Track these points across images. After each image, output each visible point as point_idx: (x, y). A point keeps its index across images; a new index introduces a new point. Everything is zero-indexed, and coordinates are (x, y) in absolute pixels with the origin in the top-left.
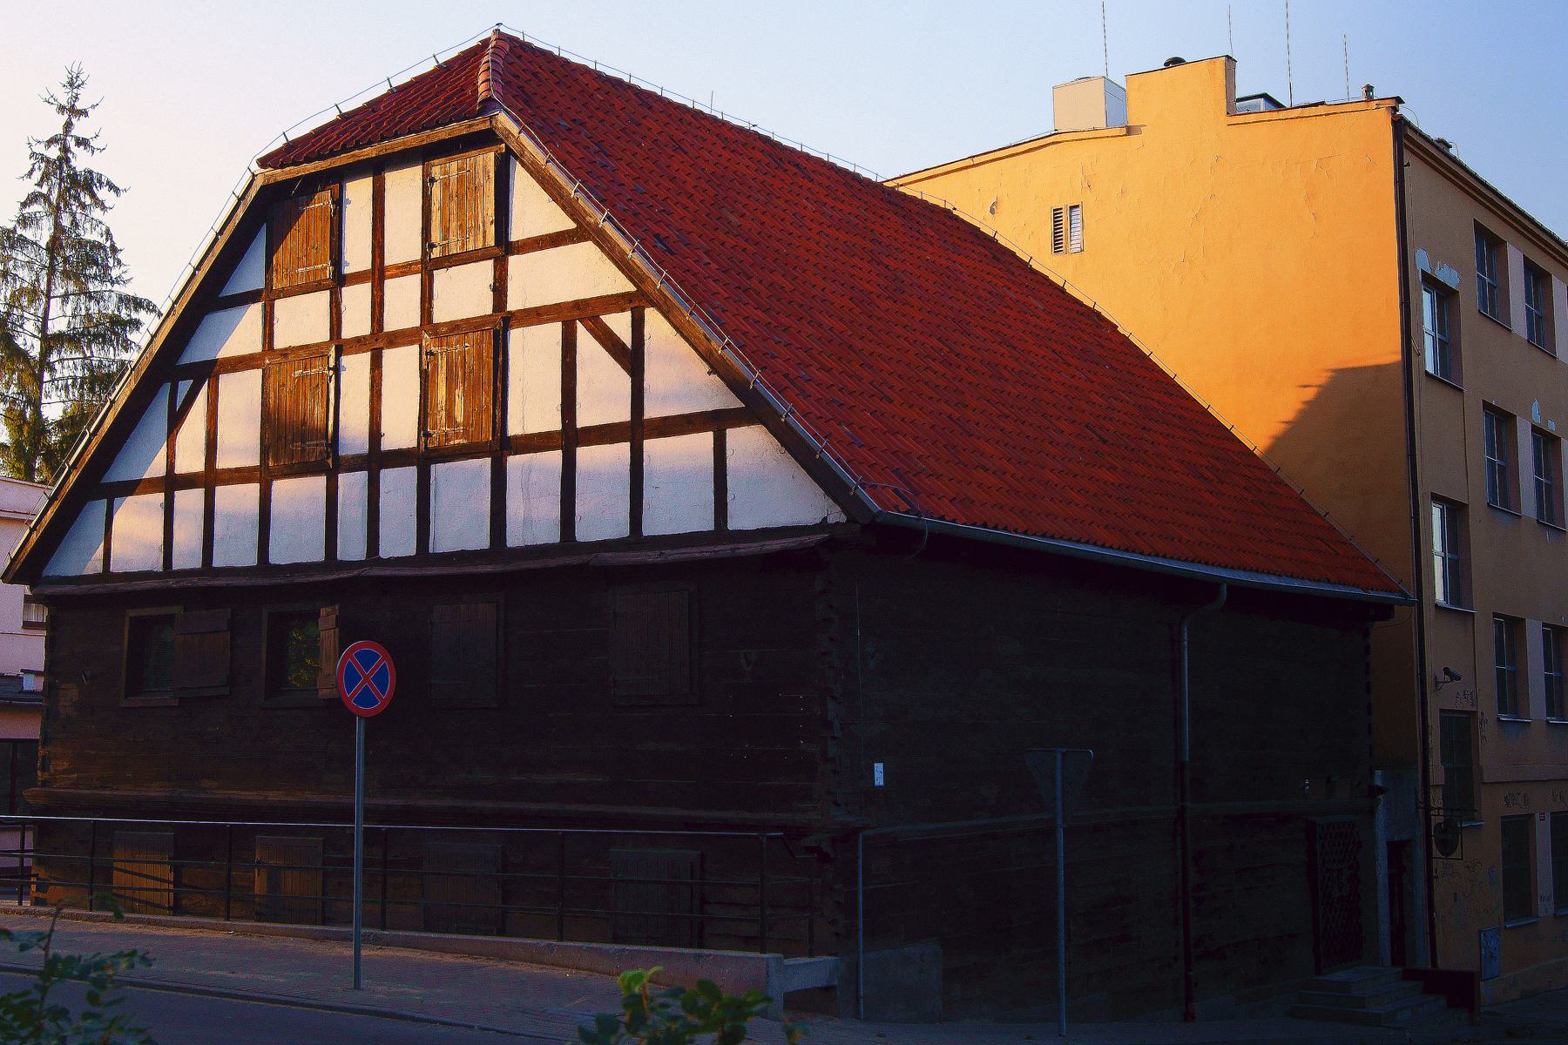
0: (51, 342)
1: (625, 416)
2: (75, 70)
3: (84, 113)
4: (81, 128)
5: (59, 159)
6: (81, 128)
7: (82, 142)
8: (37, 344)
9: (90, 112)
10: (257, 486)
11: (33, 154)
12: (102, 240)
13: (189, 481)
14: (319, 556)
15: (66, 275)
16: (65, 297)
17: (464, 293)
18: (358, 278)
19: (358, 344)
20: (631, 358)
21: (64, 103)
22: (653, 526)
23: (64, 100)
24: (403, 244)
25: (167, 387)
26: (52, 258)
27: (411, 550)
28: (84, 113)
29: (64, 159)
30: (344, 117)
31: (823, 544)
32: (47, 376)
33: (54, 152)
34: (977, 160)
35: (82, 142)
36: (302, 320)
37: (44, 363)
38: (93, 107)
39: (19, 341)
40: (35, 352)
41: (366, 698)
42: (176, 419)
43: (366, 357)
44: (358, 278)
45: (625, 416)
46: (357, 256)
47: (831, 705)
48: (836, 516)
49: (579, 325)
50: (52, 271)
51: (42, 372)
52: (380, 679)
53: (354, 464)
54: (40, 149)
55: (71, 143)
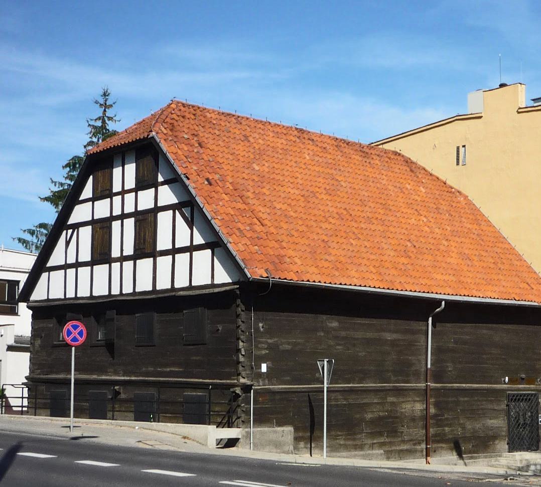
2: (106, 89)
3: (111, 106)
4: (109, 113)
5: (102, 126)
6: (109, 113)
7: (110, 119)
9: (113, 105)
11: (89, 125)
14: (107, 293)
17: (146, 200)
18: (117, 194)
21: (102, 103)
23: (102, 101)
24: (130, 183)
25: (65, 232)
27: (131, 291)
28: (111, 106)
29: (104, 127)
33: (99, 124)
34: (428, 127)
35: (110, 119)
36: (102, 209)
38: (114, 103)
41: (75, 339)
42: (68, 243)
44: (117, 194)
45: (170, 247)
46: (117, 188)
49: (177, 210)
52: (81, 334)
54: (92, 123)
55: (106, 119)
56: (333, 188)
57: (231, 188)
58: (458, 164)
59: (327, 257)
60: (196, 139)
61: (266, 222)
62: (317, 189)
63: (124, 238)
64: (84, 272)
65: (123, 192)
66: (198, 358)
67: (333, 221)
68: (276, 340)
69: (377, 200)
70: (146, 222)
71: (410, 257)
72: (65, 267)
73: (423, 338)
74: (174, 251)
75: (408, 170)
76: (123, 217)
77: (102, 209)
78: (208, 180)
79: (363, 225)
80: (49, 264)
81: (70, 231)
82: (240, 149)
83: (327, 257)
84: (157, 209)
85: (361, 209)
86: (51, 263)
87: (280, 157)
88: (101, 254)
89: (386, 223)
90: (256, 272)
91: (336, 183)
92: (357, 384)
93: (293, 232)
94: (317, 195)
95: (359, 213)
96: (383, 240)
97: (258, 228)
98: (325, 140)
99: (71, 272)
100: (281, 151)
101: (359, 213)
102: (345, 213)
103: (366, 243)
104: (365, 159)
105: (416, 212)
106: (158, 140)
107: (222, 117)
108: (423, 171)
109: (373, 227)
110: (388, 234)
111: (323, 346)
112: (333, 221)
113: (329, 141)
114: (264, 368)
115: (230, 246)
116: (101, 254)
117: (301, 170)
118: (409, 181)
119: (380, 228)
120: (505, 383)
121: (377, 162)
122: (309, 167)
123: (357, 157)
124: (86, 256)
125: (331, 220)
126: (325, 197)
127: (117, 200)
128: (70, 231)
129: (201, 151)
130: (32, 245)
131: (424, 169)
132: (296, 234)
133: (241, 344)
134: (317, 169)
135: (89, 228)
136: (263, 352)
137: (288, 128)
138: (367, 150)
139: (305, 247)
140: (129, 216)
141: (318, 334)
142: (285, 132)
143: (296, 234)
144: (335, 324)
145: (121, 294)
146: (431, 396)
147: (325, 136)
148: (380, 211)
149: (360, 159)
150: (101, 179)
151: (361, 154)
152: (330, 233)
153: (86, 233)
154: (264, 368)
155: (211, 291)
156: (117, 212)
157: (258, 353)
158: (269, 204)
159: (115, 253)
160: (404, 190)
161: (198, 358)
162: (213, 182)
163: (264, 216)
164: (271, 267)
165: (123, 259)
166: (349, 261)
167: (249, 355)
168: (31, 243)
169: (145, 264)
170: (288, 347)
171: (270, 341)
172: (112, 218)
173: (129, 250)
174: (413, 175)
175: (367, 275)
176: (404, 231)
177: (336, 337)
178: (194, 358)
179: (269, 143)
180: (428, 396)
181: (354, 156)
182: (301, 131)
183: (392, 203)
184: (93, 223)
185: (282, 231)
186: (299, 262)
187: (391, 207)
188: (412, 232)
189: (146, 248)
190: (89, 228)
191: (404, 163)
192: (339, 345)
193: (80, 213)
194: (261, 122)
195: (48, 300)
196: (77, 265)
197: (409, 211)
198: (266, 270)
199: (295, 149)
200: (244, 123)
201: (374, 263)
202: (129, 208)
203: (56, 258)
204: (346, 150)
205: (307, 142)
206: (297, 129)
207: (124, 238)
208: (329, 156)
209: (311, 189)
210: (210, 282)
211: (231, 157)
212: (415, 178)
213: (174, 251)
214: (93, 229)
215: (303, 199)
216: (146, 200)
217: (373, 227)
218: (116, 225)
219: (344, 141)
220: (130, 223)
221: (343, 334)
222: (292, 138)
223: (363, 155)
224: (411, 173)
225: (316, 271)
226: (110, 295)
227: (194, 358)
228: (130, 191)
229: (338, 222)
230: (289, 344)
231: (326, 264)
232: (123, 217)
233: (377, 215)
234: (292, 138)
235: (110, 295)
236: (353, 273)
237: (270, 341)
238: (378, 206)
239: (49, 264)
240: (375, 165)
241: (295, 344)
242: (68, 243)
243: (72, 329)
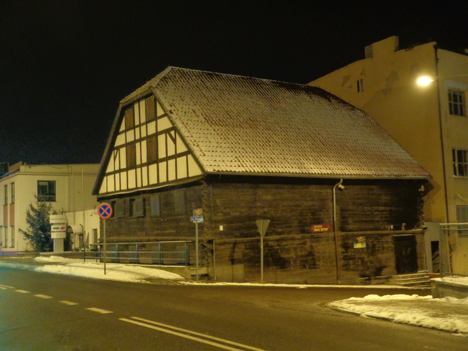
17: (152, 128)
22: (190, 175)
36: (130, 136)
42: (115, 158)
52: (108, 211)
58: (358, 91)
64: (124, 174)
65: (140, 126)
72: (114, 172)
74: (167, 158)
76: (141, 140)
77: (130, 136)
81: (116, 151)
88: (132, 165)
90: (210, 170)
92: (106, 229)
99: (117, 175)
114: (221, 228)
116: (132, 165)
120: (391, 230)
124: (124, 166)
127: (137, 130)
145: (142, 187)
146: (338, 241)
153: (123, 151)
154: (221, 228)
156: (138, 137)
159: (138, 162)
165: (142, 165)
169: (153, 168)
173: (145, 160)
180: (336, 240)
189: (153, 159)
195: (188, 178)
196: (120, 171)
213: (167, 158)
214: (126, 149)
216: (152, 128)
226: (137, 188)
232: (141, 140)
235: (137, 188)
242: (115, 158)
243: (107, 209)
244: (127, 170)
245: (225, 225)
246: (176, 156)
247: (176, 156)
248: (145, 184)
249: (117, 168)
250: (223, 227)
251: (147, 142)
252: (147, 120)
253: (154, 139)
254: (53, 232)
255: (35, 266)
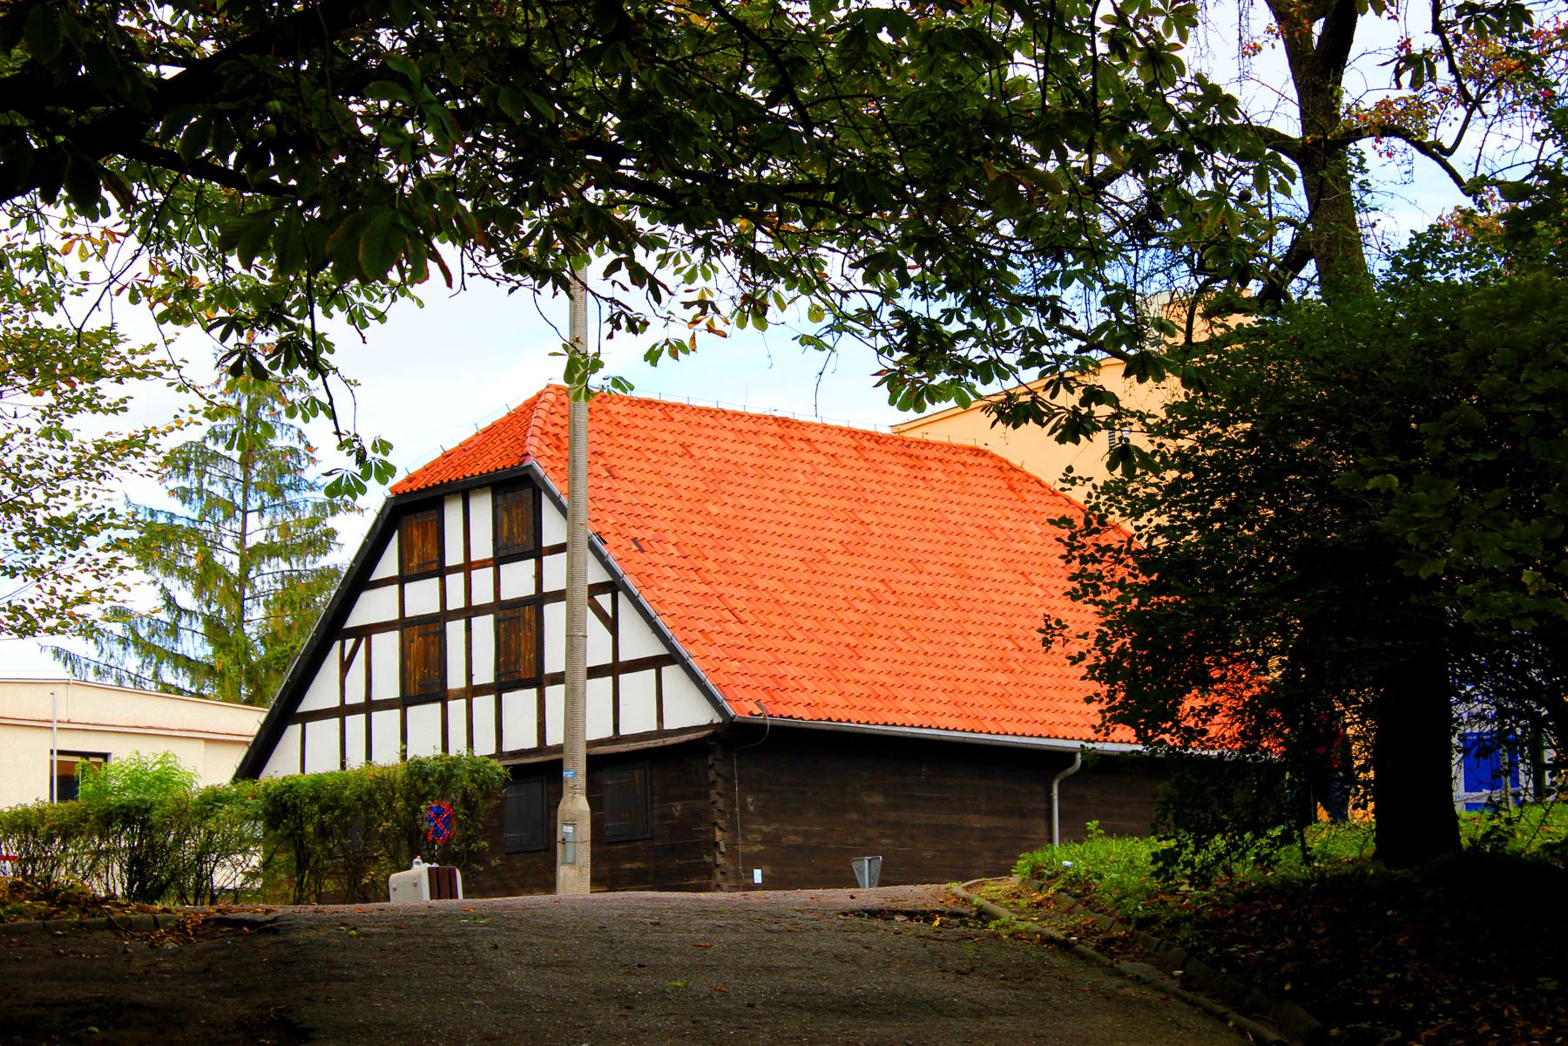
0: (252, 556)
1: (374, 714)
8: (236, 560)
10: (547, 671)
12: (295, 444)
13: (354, 709)
15: (260, 488)
16: (261, 511)
17: (518, 580)
18: (455, 569)
19: (456, 615)
20: (612, 624)
22: (670, 724)
24: (483, 547)
25: (338, 644)
26: (247, 474)
30: (446, 455)
31: (709, 736)
32: (248, 593)
36: (423, 598)
37: (244, 579)
39: (218, 559)
40: (235, 569)
42: (345, 665)
43: (462, 622)
44: (455, 569)
46: (454, 556)
47: (718, 833)
48: (718, 719)
50: (246, 485)
51: (242, 588)
53: (458, 695)
56: (855, 539)
57: (677, 554)
59: (857, 676)
60: (601, 461)
61: (744, 616)
62: (827, 545)
63: (473, 651)
65: (468, 567)
66: (637, 865)
67: (862, 606)
68: (776, 826)
69: (944, 558)
70: (519, 623)
71: (1012, 671)
72: (343, 711)
73: (1043, 824)
75: (1005, 486)
76: (470, 612)
77: (423, 598)
78: (634, 540)
79: (918, 612)
80: (303, 708)
81: (350, 643)
82: (680, 472)
83: (857, 676)
84: (540, 599)
85: (913, 578)
86: (309, 704)
87: (753, 482)
88: (424, 683)
89: (963, 604)
90: (744, 708)
91: (862, 529)
93: (793, 632)
94: (828, 555)
95: (910, 588)
96: (958, 639)
97: (735, 628)
98: (832, 438)
99: (356, 723)
100: (751, 471)
101: (910, 588)
102: (882, 588)
103: (927, 647)
104: (914, 472)
105: (1020, 578)
106: (542, 473)
107: (638, 410)
108: (1036, 487)
109: (938, 615)
110: (969, 627)
111: (858, 840)
112: (862, 606)
113: (840, 439)
115: (692, 662)
116: (424, 683)
117: (793, 508)
118: (1008, 512)
119: (950, 614)
121: (939, 475)
122: (809, 499)
123: (899, 469)
124: (388, 685)
125: (857, 604)
126: (844, 559)
128: (350, 643)
129: (616, 485)
130: (87, 666)
131: (1039, 482)
132: (798, 635)
133: (718, 833)
134: (824, 502)
135: (393, 637)
136: (756, 849)
137: (759, 418)
138: (917, 452)
139: (818, 659)
140: (482, 610)
141: (849, 816)
142: (754, 428)
143: (798, 635)
144: (878, 799)
145: (499, 754)
147: (833, 428)
148: (949, 580)
149: (904, 471)
150: (418, 542)
151: (904, 460)
152: (859, 630)
153: (387, 647)
155: (660, 742)
157: (748, 849)
158: (746, 582)
159: (456, 680)
160: (997, 532)
161: (637, 865)
162: (644, 545)
163: (741, 605)
164: (765, 697)
165: (472, 691)
166: (898, 681)
167: (732, 853)
168: (84, 661)
170: (798, 840)
171: (765, 828)
172: (445, 615)
173: (485, 673)
174: (1015, 497)
175: (933, 707)
176: (999, 619)
177: (880, 823)
178: (628, 866)
179: (727, 455)
181: (892, 468)
182: (784, 422)
183: (972, 562)
184: (403, 624)
185: (774, 632)
186: (810, 686)
187: (971, 572)
188: (1014, 620)
189: (519, 667)
190: (393, 637)
191: (995, 472)
192: (884, 836)
193: (374, 607)
194: (709, 410)
195: (661, 733)
196: (370, 706)
197: (1009, 576)
198: (758, 702)
199: (777, 463)
200: (677, 417)
201: (943, 684)
202: (482, 595)
203: (323, 693)
204: (874, 455)
205: (799, 445)
206: (776, 419)
207: (473, 651)
208: (843, 473)
209: (816, 545)
210: (654, 728)
211: (666, 492)
212: (1019, 505)
214: (402, 637)
215: (803, 567)
217: (938, 615)
218: (455, 629)
219: (865, 433)
220: (484, 626)
221: (892, 816)
222: (768, 440)
223: (911, 463)
224: (1010, 494)
225: (840, 701)
227: (628, 866)
228: (483, 564)
229: (871, 608)
230: (797, 833)
231: (858, 689)
232: (470, 612)
233: (943, 590)
234: (768, 440)
236: (906, 704)
237: (765, 828)
238: (945, 570)
239: (303, 708)
240: (935, 484)
241: (808, 835)
244: (404, 702)
245: (767, 868)
246: (615, 669)
247: (615, 669)
248: (485, 745)
249: (356, 696)
250: (752, 877)
251: (497, 622)
252: (502, 554)
253: (413, 690)
254: (159, 611)
255: (255, 910)
